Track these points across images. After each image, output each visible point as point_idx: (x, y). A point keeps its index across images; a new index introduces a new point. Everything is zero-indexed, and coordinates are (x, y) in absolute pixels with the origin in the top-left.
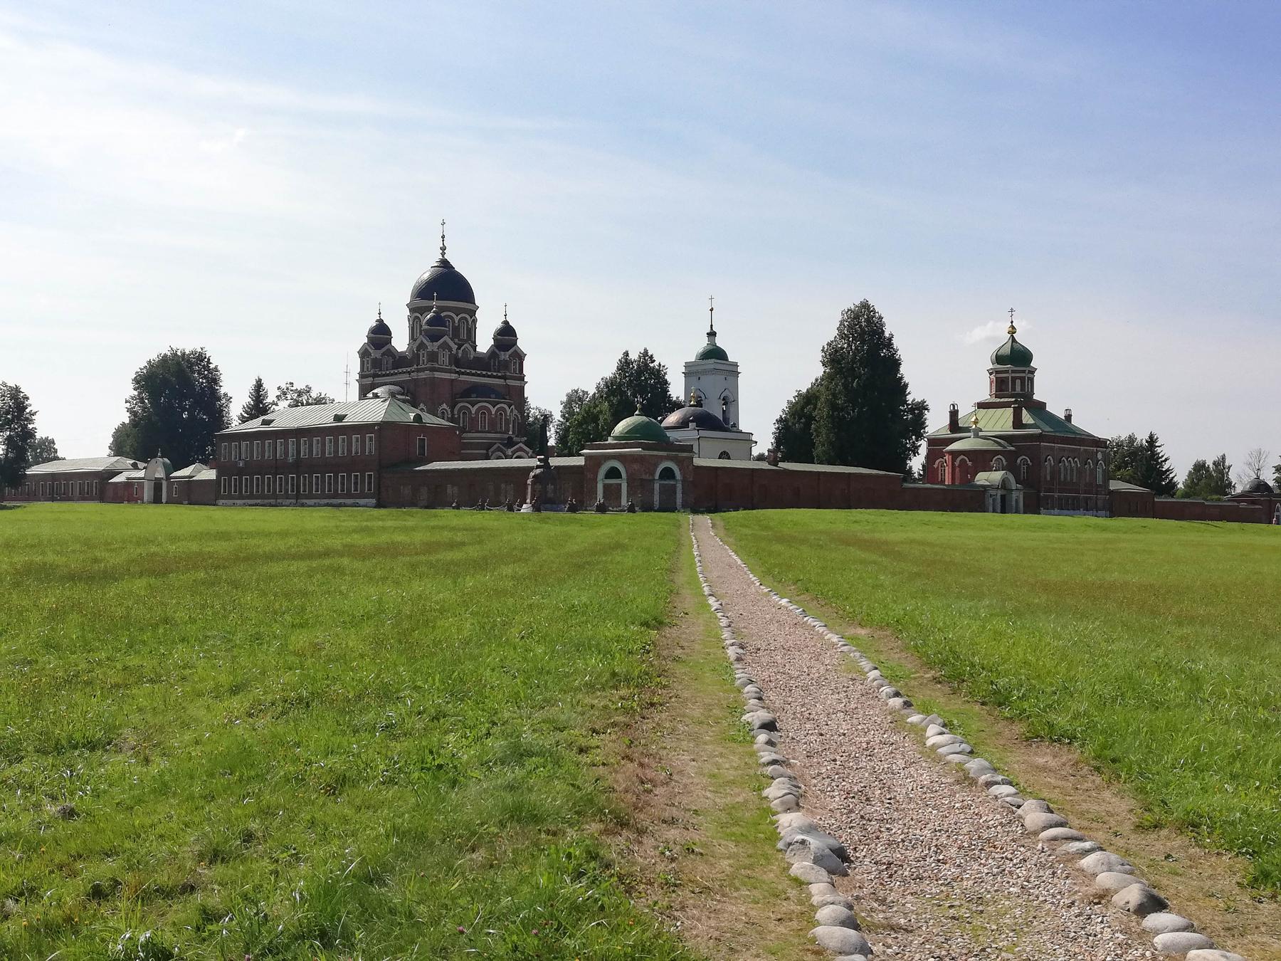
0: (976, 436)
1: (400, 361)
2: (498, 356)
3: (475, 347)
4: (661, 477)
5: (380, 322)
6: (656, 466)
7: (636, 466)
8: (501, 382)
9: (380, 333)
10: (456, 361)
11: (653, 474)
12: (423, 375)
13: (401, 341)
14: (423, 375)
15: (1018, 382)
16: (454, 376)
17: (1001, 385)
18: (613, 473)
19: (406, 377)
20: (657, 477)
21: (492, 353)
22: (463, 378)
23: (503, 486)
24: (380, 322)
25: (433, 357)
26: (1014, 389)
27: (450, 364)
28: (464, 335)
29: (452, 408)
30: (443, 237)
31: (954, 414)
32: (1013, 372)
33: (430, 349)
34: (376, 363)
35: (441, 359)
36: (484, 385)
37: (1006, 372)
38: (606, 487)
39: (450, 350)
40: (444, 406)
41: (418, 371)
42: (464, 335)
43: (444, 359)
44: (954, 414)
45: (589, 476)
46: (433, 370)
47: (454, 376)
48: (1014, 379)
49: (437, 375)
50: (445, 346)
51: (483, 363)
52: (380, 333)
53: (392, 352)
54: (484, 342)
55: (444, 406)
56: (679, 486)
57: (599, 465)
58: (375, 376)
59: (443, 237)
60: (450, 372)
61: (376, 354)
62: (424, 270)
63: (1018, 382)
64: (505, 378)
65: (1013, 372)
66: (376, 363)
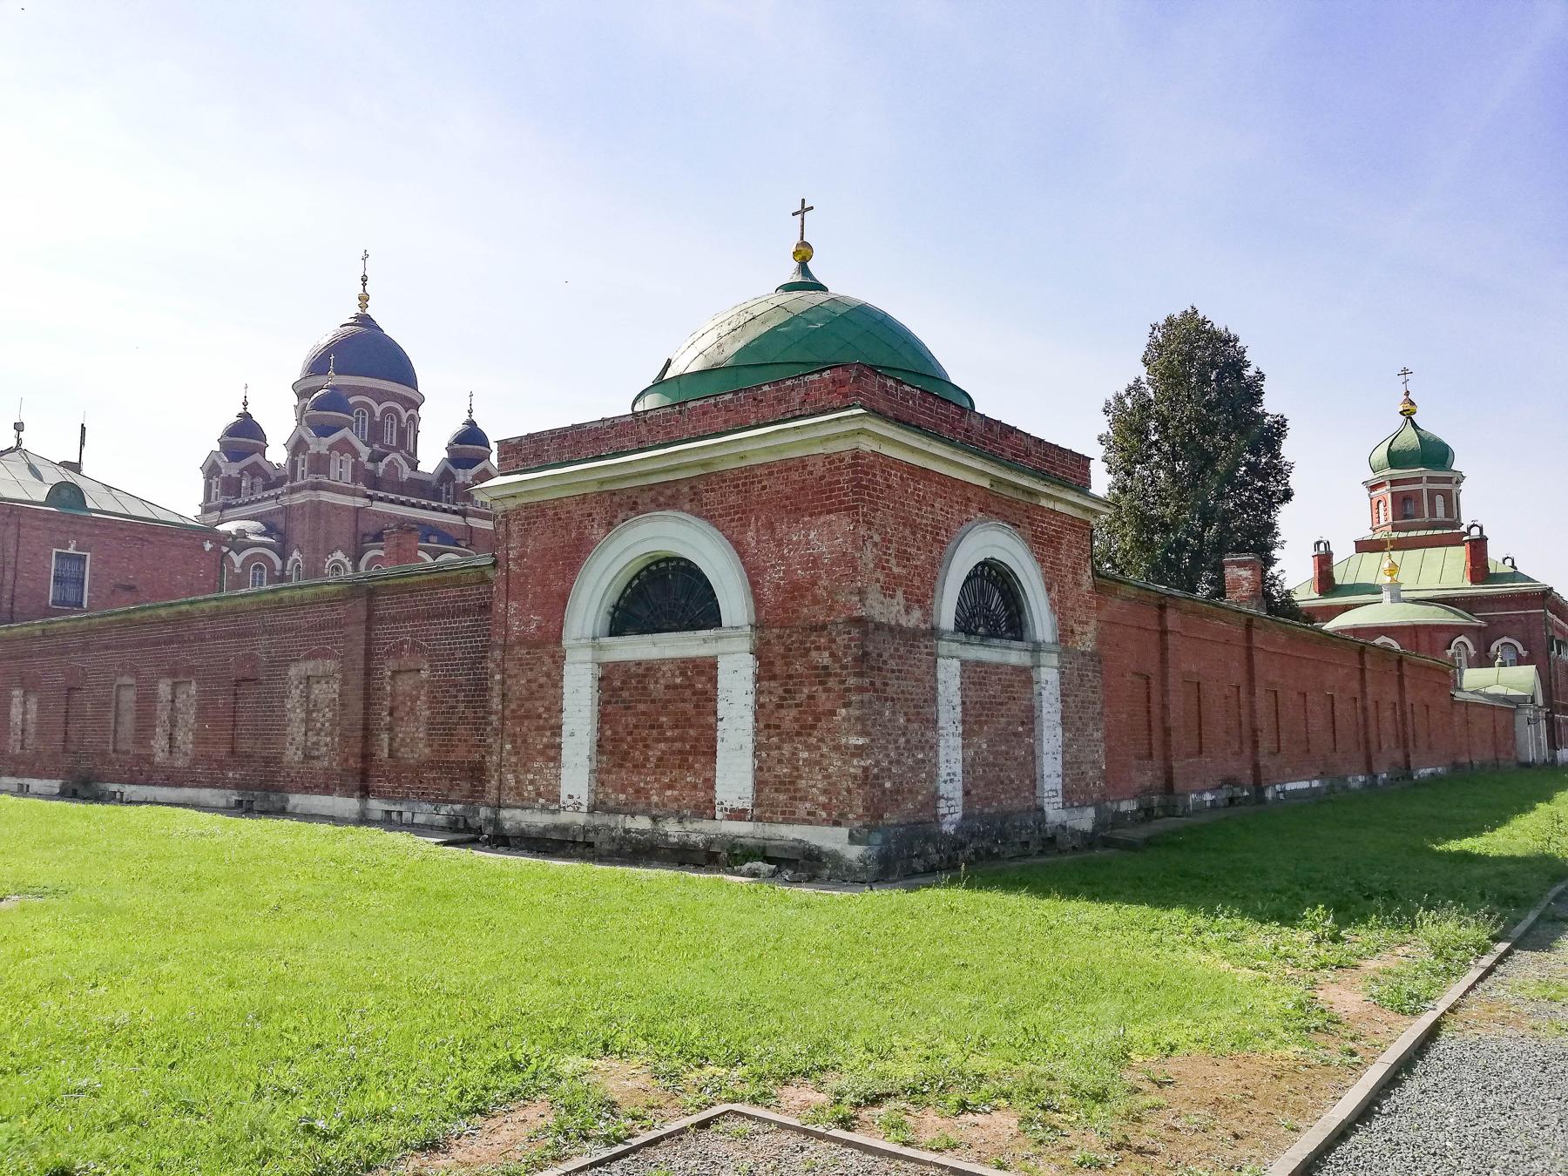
0: (1396, 598)
1: (271, 480)
2: (453, 478)
3: (414, 465)
4: (966, 626)
5: (246, 417)
6: (941, 541)
7: (824, 537)
8: (457, 520)
9: (244, 434)
10: (358, 472)
11: (923, 598)
12: (299, 499)
13: (277, 454)
14: (299, 499)
15: (1439, 499)
16: (360, 502)
17: (1404, 505)
18: (666, 596)
19: (270, 506)
20: (947, 616)
21: (445, 475)
22: (379, 506)
23: (164, 688)
24: (246, 417)
25: (320, 464)
26: (1433, 513)
27: (354, 479)
28: (391, 438)
29: (356, 560)
30: (364, 280)
31: (1324, 561)
32: (1431, 480)
33: (313, 449)
34: (232, 486)
35: (334, 470)
36: (422, 524)
37: (1418, 480)
38: (616, 686)
39: (356, 454)
40: (339, 555)
41: (293, 491)
42: (391, 438)
43: (341, 469)
44: (1324, 561)
45: (518, 619)
46: (316, 487)
47: (360, 502)
48: (1432, 494)
49: (326, 496)
50: (345, 447)
51: (424, 489)
52: (244, 434)
53: (257, 470)
54: (431, 454)
55: (339, 555)
56: (1049, 676)
57: (574, 555)
58: (227, 506)
59: (364, 280)
60: (354, 493)
61: (231, 469)
62: (327, 323)
63: (1439, 499)
64: (464, 514)
65: (1431, 480)
66: (232, 486)
